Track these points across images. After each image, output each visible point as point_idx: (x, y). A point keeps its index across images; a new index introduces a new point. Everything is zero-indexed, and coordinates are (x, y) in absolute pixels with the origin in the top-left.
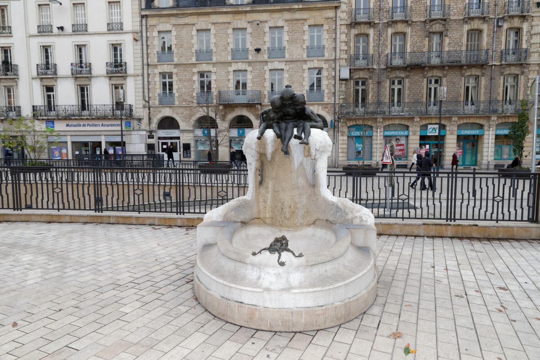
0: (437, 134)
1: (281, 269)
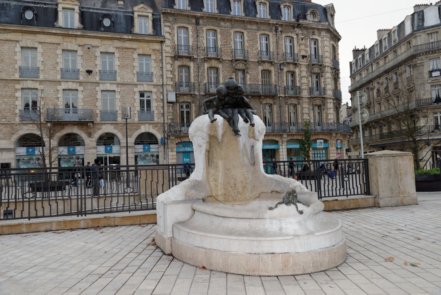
1: (301, 217)
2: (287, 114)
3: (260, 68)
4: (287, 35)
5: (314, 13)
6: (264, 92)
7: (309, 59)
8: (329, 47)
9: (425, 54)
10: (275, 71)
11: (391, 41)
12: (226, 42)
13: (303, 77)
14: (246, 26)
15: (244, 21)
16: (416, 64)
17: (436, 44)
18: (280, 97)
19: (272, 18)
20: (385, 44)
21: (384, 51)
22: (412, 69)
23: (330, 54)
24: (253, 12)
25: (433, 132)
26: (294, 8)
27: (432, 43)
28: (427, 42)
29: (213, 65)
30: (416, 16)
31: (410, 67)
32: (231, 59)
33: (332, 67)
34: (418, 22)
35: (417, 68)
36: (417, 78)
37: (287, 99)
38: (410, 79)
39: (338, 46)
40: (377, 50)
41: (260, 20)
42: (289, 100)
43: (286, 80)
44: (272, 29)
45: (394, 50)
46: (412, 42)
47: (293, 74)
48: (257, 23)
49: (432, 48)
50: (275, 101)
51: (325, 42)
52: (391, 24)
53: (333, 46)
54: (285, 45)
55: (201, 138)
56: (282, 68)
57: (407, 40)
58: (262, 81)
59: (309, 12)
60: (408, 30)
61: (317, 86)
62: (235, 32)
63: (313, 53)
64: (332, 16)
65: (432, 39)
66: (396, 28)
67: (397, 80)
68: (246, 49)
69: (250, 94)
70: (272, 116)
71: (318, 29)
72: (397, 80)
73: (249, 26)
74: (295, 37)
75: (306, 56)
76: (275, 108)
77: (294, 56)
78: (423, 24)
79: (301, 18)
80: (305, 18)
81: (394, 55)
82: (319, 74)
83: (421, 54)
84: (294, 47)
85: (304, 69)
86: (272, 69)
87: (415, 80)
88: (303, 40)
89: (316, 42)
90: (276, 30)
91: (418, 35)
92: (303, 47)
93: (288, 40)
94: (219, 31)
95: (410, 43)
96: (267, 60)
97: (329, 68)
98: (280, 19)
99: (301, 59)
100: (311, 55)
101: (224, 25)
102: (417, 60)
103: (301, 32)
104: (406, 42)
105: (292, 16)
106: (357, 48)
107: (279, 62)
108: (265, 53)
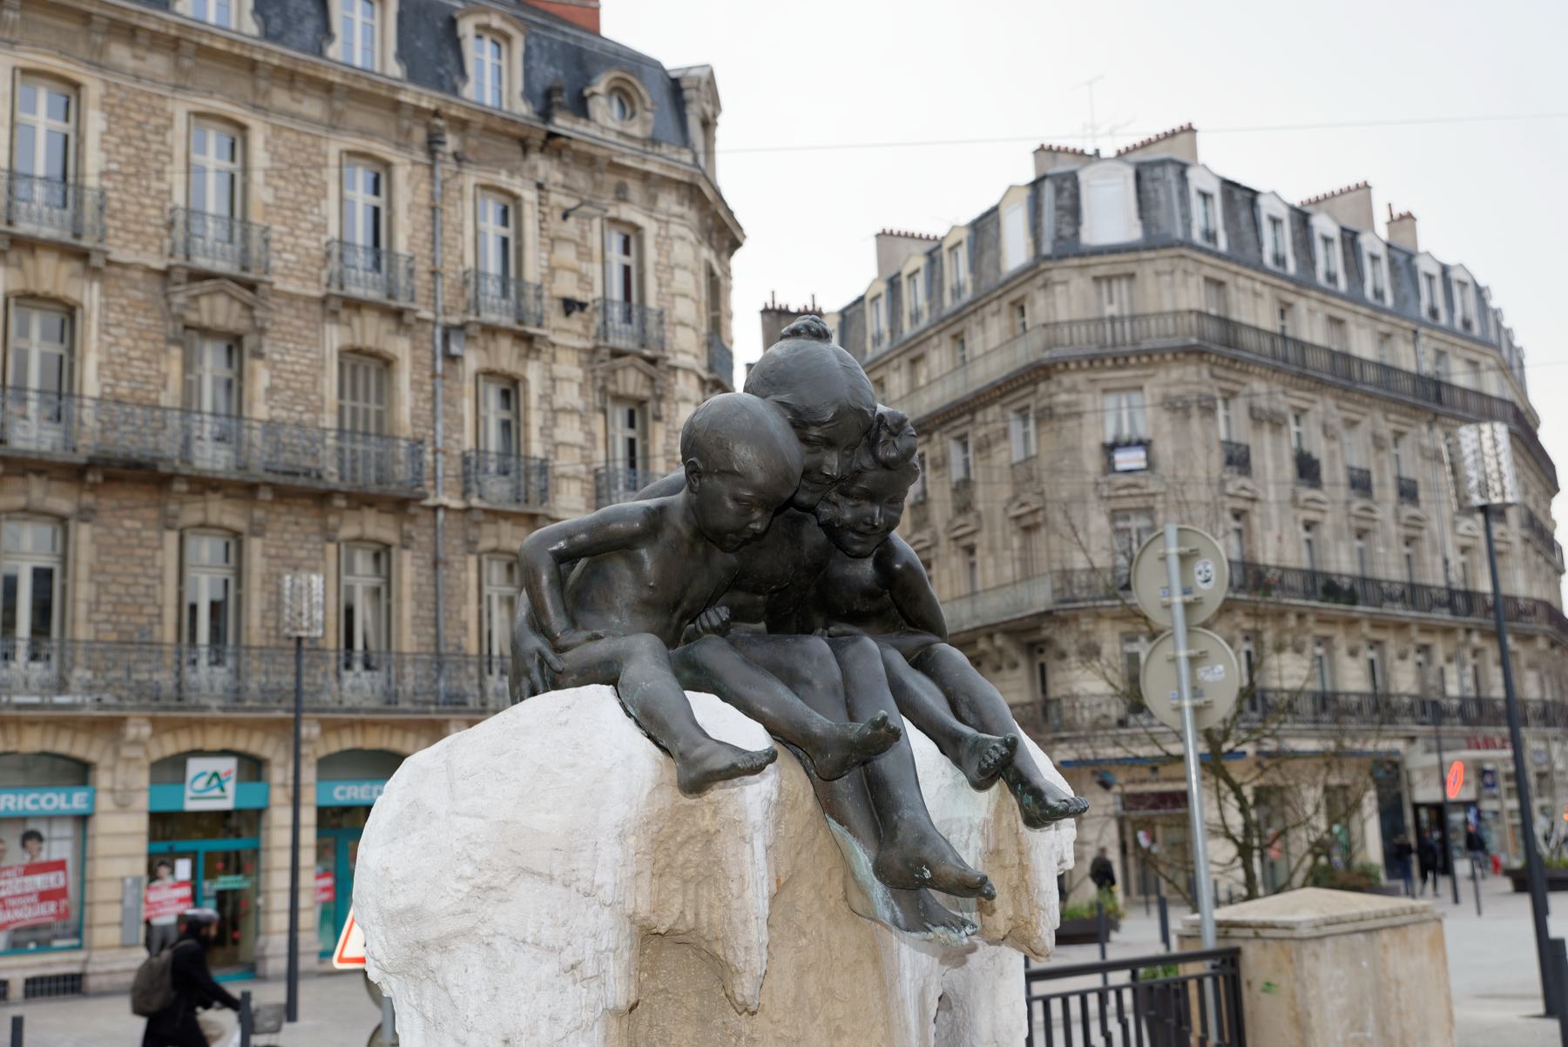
0: (227, 804)
2: (472, 607)
3: (335, 337)
4: (487, 177)
5: (628, 95)
6: (348, 474)
7: (598, 319)
8: (694, 273)
9: (1085, 364)
10: (416, 362)
11: (941, 290)
12: (141, 166)
13: (564, 410)
14: (267, 94)
15: (253, 66)
16: (1050, 408)
17: (1127, 325)
18: (435, 509)
19: (413, 76)
20: (915, 296)
21: (907, 329)
22: (1032, 423)
23: (698, 311)
24: (310, 25)
25: (1122, 723)
26: (528, 49)
27: (1113, 319)
28: (1092, 314)
29: (46, 286)
30: (1048, 190)
31: (1025, 419)
32: (159, 264)
33: (705, 375)
34: (1058, 221)
35: (1056, 425)
36: (1055, 471)
37: (477, 524)
38: (1025, 474)
39: (727, 274)
40: (877, 320)
41: (345, 75)
42: (489, 529)
43: (471, 421)
44: (409, 133)
45: (956, 329)
46: (1033, 303)
47: (511, 390)
48: (328, 88)
49: (1114, 345)
50: (407, 526)
51: (678, 245)
52: (943, 214)
53: (711, 274)
54: (475, 232)
55: (549, 968)
56: (454, 349)
57: (1011, 294)
58: (341, 409)
59: (601, 85)
60: (1016, 250)
61: (632, 464)
62: (199, 115)
63: (617, 293)
64: (708, 125)
65: (1111, 302)
66: (964, 235)
67: (967, 470)
68: (256, 217)
69: (270, 478)
70: (386, 617)
71: (645, 176)
72: (967, 470)
73: (281, 98)
74: (529, 195)
75: (582, 306)
76: (409, 569)
77: (520, 294)
78: (1076, 234)
79: (561, 106)
80: (581, 108)
81: (954, 354)
82: (642, 403)
83: (1072, 366)
84: (520, 250)
85: (569, 368)
86: (400, 347)
87: (1045, 475)
88: (571, 220)
89: (631, 238)
90: (433, 144)
91: (1056, 275)
92: (567, 254)
93: (492, 209)
94: (94, 88)
95: (1022, 309)
96: (372, 297)
97: (694, 381)
98: (455, 91)
99: (555, 318)
100: (606, 301)
101: (131, 63)
102: (1053, 388)
103: (558, 176)
104: (1005, 302)
105: (519, 85)
106: (781, 302)
107: (441, 319)
108: (362, 260)
